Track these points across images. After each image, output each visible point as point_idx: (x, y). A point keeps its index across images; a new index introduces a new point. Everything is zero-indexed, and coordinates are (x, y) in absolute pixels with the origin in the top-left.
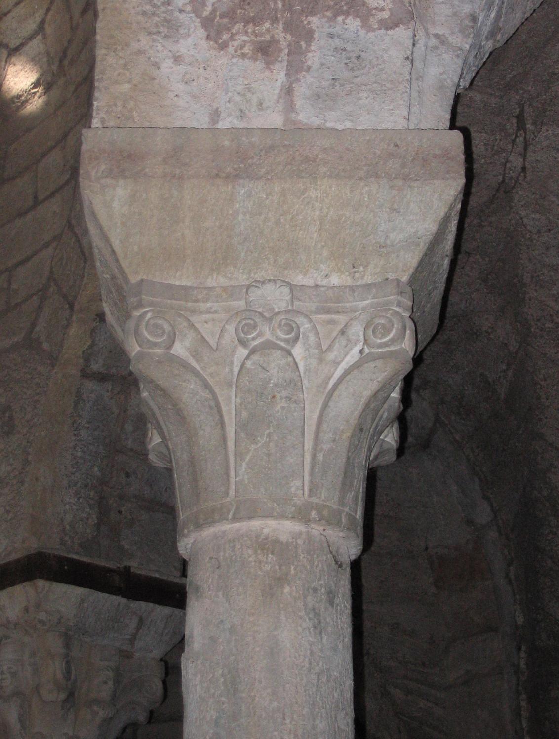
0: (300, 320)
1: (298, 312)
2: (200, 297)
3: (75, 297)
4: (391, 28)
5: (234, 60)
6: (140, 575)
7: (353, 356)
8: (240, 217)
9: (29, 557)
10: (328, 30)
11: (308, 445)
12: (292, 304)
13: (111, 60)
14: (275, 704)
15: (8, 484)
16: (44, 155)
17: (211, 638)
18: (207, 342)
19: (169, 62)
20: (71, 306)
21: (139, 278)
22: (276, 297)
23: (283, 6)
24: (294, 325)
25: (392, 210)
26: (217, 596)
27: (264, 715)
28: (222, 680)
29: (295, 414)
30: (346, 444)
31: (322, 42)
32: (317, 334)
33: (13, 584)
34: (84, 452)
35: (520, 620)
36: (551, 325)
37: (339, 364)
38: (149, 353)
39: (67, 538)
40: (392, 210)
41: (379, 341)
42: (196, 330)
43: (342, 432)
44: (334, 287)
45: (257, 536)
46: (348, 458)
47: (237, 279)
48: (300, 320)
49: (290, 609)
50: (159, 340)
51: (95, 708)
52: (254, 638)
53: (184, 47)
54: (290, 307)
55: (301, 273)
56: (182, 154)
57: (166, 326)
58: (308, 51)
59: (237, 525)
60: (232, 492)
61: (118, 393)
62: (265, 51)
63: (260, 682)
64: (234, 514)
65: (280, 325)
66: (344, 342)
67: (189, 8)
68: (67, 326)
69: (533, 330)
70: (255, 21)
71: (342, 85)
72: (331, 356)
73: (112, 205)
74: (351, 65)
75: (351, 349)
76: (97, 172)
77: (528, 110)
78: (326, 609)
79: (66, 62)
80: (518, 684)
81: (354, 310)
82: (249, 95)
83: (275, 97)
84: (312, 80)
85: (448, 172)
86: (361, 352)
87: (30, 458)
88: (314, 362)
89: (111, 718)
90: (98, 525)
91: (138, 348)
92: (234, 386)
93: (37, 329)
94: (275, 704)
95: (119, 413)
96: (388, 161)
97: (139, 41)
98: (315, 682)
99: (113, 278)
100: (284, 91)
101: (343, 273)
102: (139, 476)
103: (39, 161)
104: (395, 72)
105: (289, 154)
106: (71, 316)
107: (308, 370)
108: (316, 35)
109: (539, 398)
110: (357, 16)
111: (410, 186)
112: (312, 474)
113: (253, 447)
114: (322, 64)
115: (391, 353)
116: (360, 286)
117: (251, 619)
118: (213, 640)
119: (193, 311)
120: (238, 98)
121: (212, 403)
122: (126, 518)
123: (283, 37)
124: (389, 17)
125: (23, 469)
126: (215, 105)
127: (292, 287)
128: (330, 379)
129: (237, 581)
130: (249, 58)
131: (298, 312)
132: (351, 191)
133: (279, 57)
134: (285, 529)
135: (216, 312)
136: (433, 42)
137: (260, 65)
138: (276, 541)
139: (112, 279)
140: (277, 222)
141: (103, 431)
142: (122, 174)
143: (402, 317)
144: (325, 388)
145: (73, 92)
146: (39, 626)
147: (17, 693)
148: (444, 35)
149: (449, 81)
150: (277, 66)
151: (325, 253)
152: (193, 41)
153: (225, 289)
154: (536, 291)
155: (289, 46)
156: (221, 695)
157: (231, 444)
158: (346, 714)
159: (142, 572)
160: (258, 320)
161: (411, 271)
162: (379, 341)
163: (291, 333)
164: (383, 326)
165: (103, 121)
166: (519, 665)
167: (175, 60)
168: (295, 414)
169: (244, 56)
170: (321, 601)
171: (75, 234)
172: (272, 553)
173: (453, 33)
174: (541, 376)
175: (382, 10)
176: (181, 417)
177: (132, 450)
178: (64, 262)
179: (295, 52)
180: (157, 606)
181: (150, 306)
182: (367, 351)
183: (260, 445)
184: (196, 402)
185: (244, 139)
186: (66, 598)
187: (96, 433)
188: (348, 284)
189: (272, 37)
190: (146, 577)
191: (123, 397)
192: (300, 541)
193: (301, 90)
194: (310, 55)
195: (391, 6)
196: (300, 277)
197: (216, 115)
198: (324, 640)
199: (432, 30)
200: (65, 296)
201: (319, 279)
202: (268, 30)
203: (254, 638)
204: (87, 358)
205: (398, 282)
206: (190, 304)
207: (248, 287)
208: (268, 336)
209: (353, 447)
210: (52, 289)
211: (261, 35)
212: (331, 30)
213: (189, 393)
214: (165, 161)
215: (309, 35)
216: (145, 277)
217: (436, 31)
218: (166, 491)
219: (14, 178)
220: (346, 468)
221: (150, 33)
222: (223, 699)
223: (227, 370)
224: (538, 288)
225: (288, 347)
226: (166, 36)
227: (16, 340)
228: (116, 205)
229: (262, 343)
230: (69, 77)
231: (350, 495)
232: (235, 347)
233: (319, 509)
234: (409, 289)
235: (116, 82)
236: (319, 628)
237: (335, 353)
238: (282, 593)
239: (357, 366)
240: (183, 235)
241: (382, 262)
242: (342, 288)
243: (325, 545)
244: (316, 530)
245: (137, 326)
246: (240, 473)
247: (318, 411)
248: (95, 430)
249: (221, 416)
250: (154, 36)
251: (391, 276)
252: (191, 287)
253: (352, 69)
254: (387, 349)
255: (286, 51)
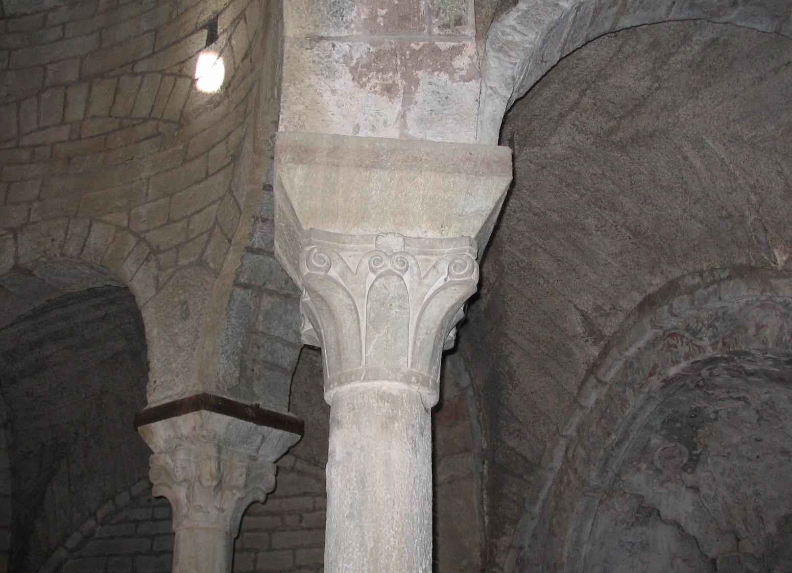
0: (409, 258)
1: (407, 253)
2: (346, 240)
3: (233, 236)
4: (467, 81)
5: (370, 95)
6: (265, 410)
7: (440, 282)
8: (374, 192)
9: (197, 396)
10: (429, 80)
11: (411, 336)
12: (404, 248)
13: (292, 89)
14: (389, 496)
15: (184, 350)
16: (213, 146)
17: (348, 453)
18: (350, 269)
19: (329, 93)
20: (230, 241)
21: (309, 227)
22: (394, 243)
23: (401, 63)
24: (405, 261)
25: (467, 193)
26: (352, 427)
27: (382, 503)
28: (355, 479)
29: (404, 316)
30: (434, 336)
31: (425, 87)
32: (418, 268)
33: (187, 412)
34: (233, 332)
35: (485, 446)
36: (517, 268)
37: (431, 286)
38: (315, 274)
39: (220, 385)
40: (467, 193)
41: (457, 273)
42: (344, 261)
43: (432, 329)
44: (429, 239)
45: (379, 391)
46: (434, 345)
47: (369, 230)
48: (409, 258)
49: (399, 438)
50: (321, 266)
51: (234, 491)
52: (376, 454)
53: (338, 84)
54: (403, 250)
55: (409, 228)
56: (336, 151)
57: (326, 258)
58: (416, 92)
59: (366, 384)
60: (363, 363)
61: (256, 296)
62: (389, 90)
63: (380, 482)
64: (364, 377)
65: (397, 260)
66: (435, 273)
67: (342, 60)
68: (226, 254)
69: (505, 270)
70: (384, 71)
71: (436, 114)
72: (427, 281)
73: (293, 181)
74: (442, 102)
75: (439, 278)
76: (285, 159)
77: (516, 137)
78: (419, 438)
79: (230, 90)
80: (482, 484)
81: (442, 254)
82: (378, 117)
83: (395, 119)
84: (418, 110)
85: (502, 172)
86: (445, 280)
87: (199, 334)
88: (416, 285)
89: (243, 498)
90: (239, 379)
91: (308, 271)
92: (366, 297)
93: (206, 254)
94: (389, 496)
95: (255, 309)
96: (464, 163)
97: (310, 79)
98: (412, 483)
99: (288, 226)
100: (400, 115)
101: (435, 230)
102: (266, 348)
103: (209, 150)
104: (468, 108)
105: (403, 156)
106: (229, 247)
107: (412, 289)
108: (421, 82)
109: (506, 312)
110: (447, 72)
111: (479, 179)
112: (413, 353)
113: (377, 336)
114: (424, 101)
115: (465, 282)
116: (446, 239)
117: (374, 442)
118: (349, 454)
119: (342, 250)
120: (371, 118)
121: (353, 308)
122: (256, 374)
123: (401, 83)
124: (467, 74)
125: (195, 341)
126: (357, 122)
127: (405, 238)
128: (425, 295)
129: (365, 418)
130: (379, 94)
131: (407, 253)
132: (443, 180)
133: (397, 94)
134: (396, 387)
135: (356, 250)
136: (489, 91)
137: (385, 98)
138: (390, 395)
139: (287, 226)
140: (397, 197)
141: (245, 320)
142: (301, 161)
143: (472, 260)
144: (422, 301)
145: (235, 108)
146: (202, 439)
147: (185, 480)
148: (495, 88)
149: (498, 116)
150: (397, 100)
151: (425, 218)
152: (344, 81)
153: (362, 236)
154: (510, 246)
155: (404, 88)
156: (354, 489)
157: (363, 333)
158: (429, 503)
159: (267, 408)
160: (383, 256)
161: (477, 231)
162: (457, 273)
163: (403, 266)
164: (461, 264)
165: (286, 127)
166: (483, 473)
167: (332, 92)
168: (404, 316)
169: (375, 92)
170: (416, 433)
171: (234, 197)
172: (388, 402)
173: (501, 87)
174: (509, 299)
175: (462, 69)
176: (331, 313)
177: (262, 332)
178: (226, 213)
179: (408, 92)
180: (274, 429)
181: (316, 244)
182: (449, 279)
183: (382, 334)
184: (342, 306)
185: (377, 144)
186: (220, 422)
187: (241, 321)
188: (439, 237)
189: (394, 81)
190: (268, 411)
191: (258, 299)
192: (405, 395)
193: (411, 116)
194: (417, 94)
195: (467, 67)
196: (409, 231)
197: (357, 128)
198: (418, 457)
199: (488, 84)
200: (226, 235)
201: (420, 233)
202: (391, 77)
203: (376, 454)
204: (238, 274)
205: (470, 238)
206: (340, 245)
207: (377, 237)
208: (389, 267)
209: (437, 338)
210: (216, 230)
211: (387, 80)
212: (430, 80)
213: (338, 300)
214: (328, 155)
215: (417, 82)
216: (312, 227)
217: (490, 85)
218: (281, 358)
219: (192, 160)
220: (433, 350)
221: (317, 74)
222: (356, 491)
223: (362, 287)
224: (511, 244)
225: (402, 275)
226: (327, 77)
227: (192, 260)
228: (296, 180)
229: (385, 271)
230: (231, 99)
231: (433, 371)
232: (368, 273)
233: (417, 376)
234: (476, 242)
235: (295, 104)
236: (415, 450)
237: (429, 280)
238: (393, 427)
239: (443, 288)
240: (337, 201)
241: (460, 225)
242: (434, 239)
243: (419, 398)
244: (414, 388)
245: (308, 256)
246: (369, 352)
247: (417, 315)
248: (240, 319)
249: (358, 315)
250: (320, 76)
251: (465, 234)
252: (340, 234)
253: (443, 105)
254: (462, 279)
255: (402, 91)
